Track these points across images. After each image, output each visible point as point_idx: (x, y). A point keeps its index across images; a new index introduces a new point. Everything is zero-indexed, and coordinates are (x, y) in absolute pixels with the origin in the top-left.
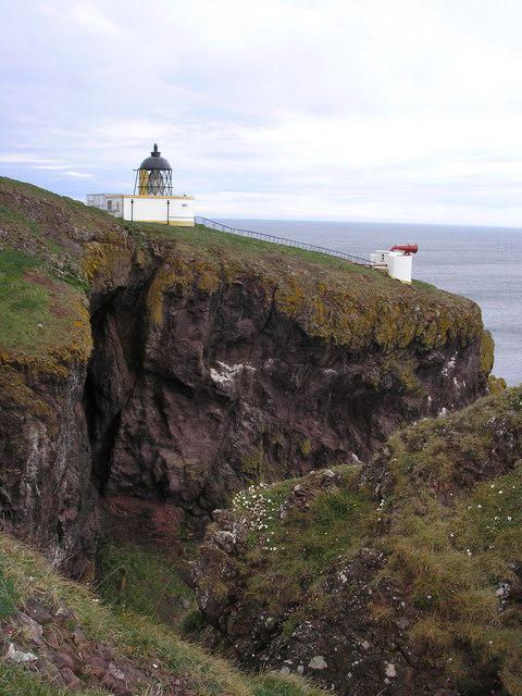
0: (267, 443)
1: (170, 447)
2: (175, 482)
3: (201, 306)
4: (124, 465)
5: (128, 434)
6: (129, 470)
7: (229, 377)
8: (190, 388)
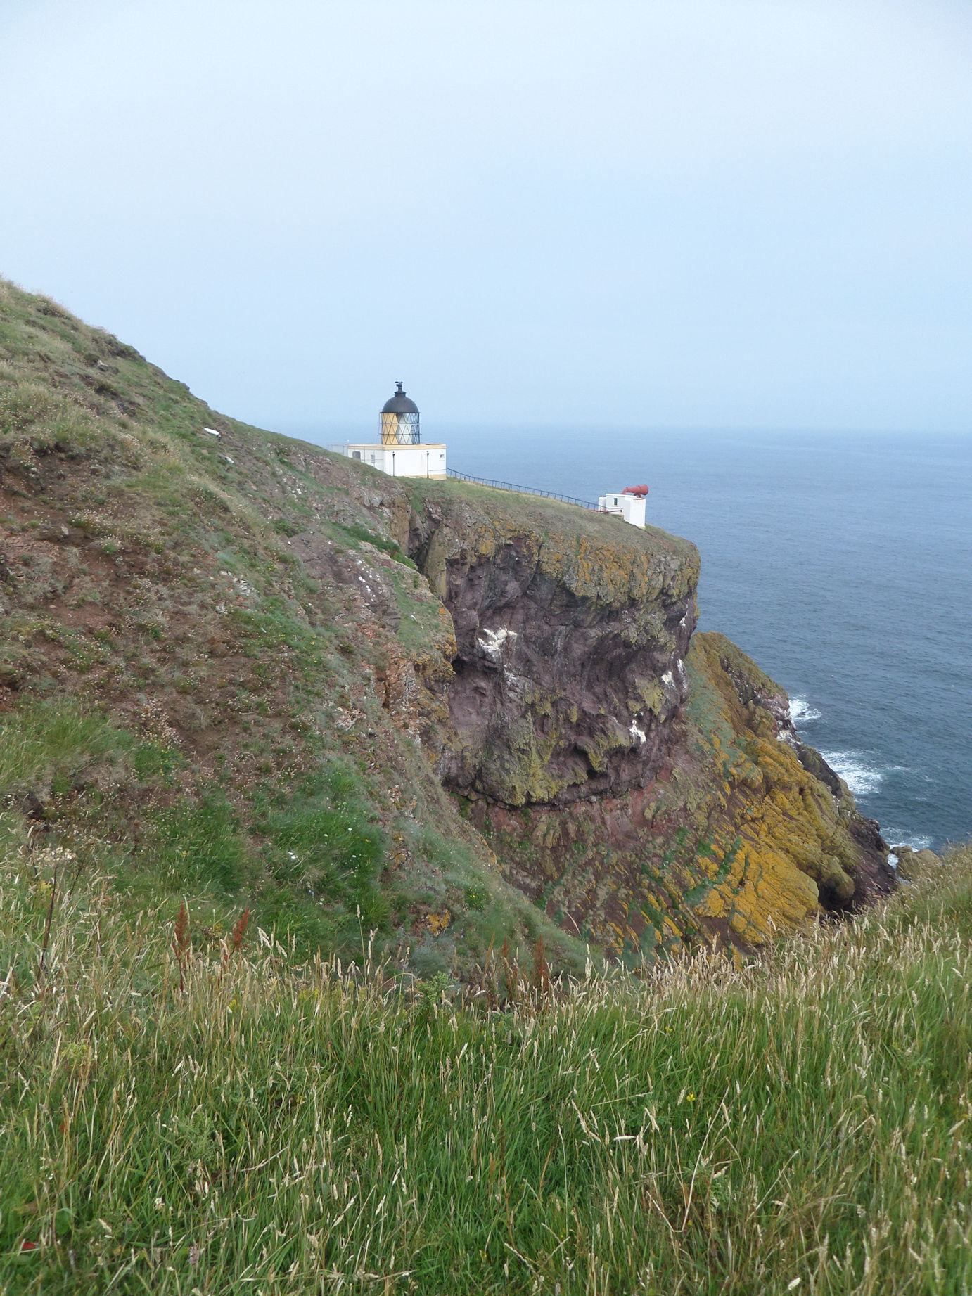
0: (535, 714)
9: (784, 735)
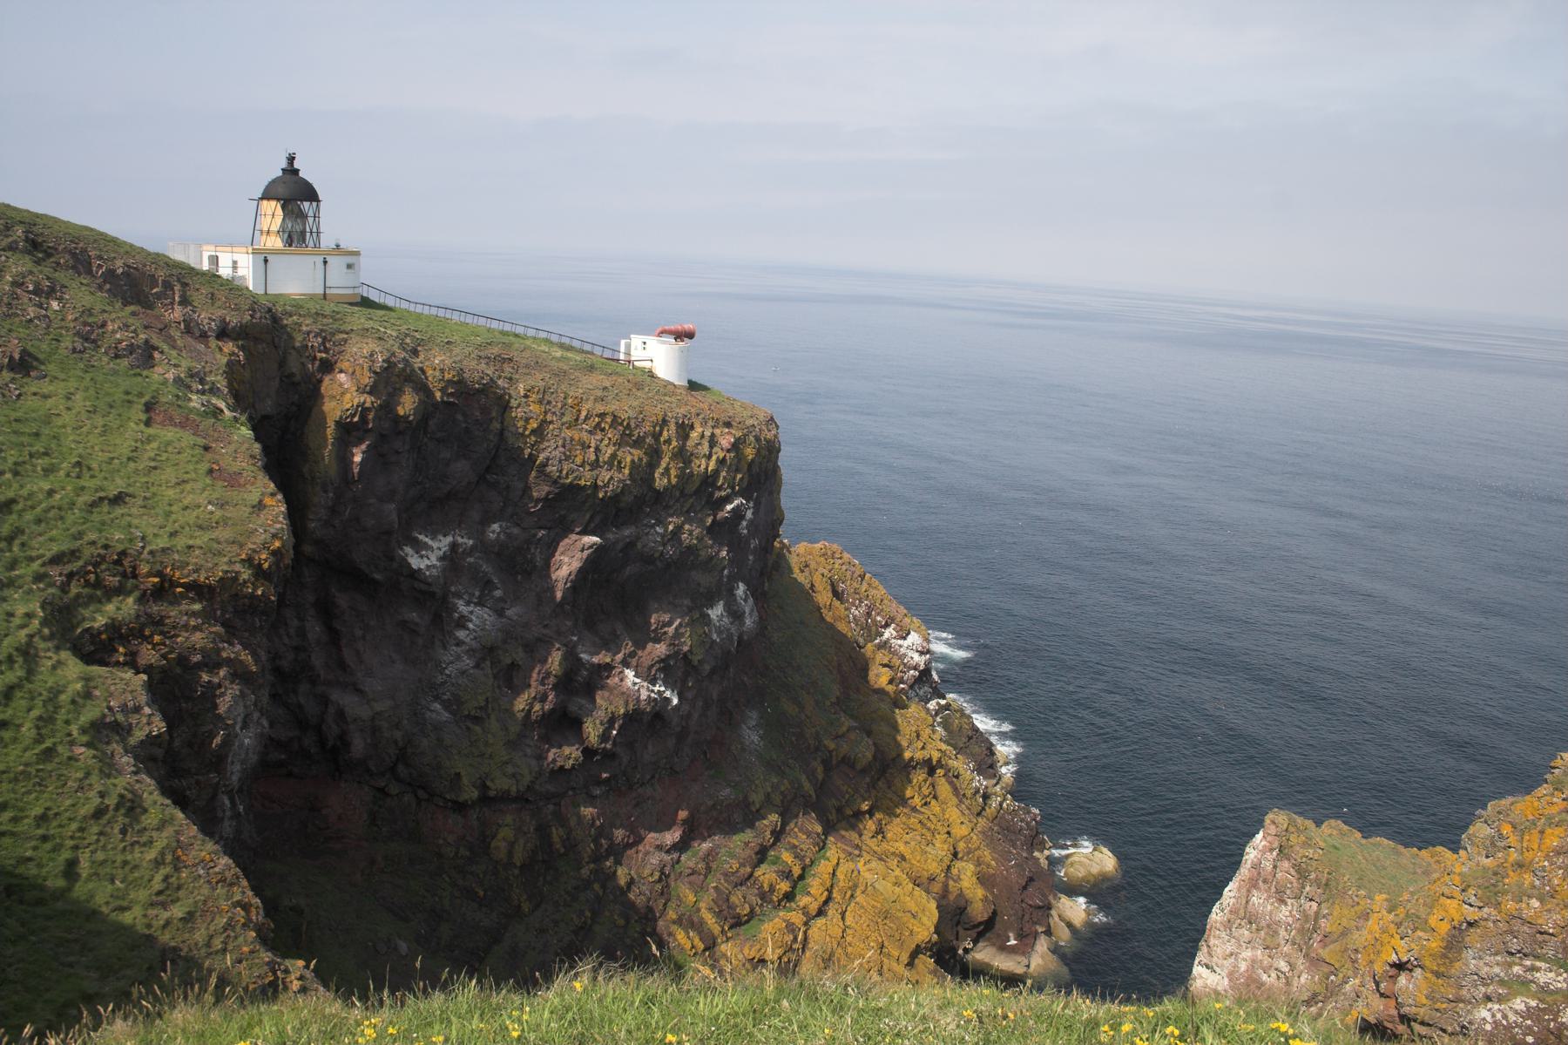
2: (358, 746)
7: (434, 560)
8: (375, 581)
9: (865, 807)
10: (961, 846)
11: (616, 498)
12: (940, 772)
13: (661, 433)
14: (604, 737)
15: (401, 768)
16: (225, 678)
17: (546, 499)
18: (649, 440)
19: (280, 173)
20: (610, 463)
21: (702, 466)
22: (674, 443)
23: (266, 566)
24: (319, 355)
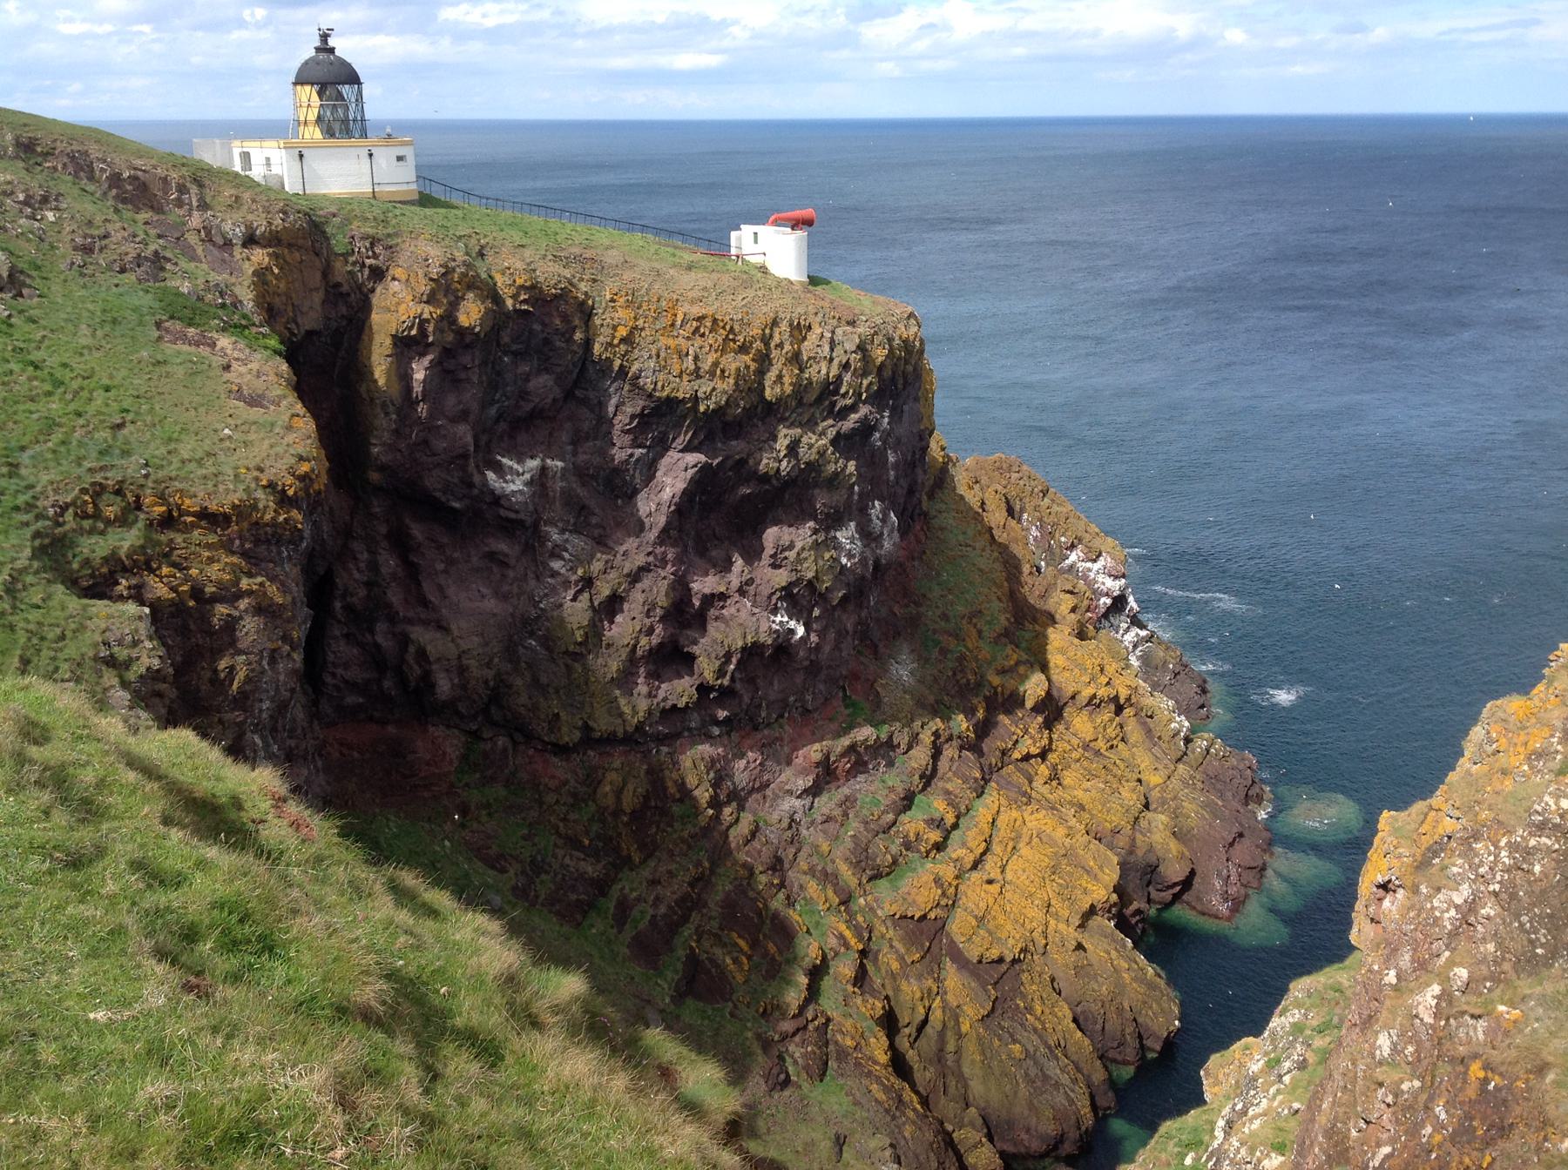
1: (425, 623)
2: (444, 685)
3: (466, 359)
4: (346, 666)
5: (348, 608)
6: (356, 674)
10: (1155, 795)
11: (720, 411)
12: (1128, 712)
13: (771, 336)
14: (721, 673)
15: (493, 709)
16: (246, 611)
17: (641, 415)
18: (758, 345)
19: (312, 53)
20: (712, 374)
21: (819, 372)
22: (787, 347)
23: (291, 492)
24: (368, 262)
